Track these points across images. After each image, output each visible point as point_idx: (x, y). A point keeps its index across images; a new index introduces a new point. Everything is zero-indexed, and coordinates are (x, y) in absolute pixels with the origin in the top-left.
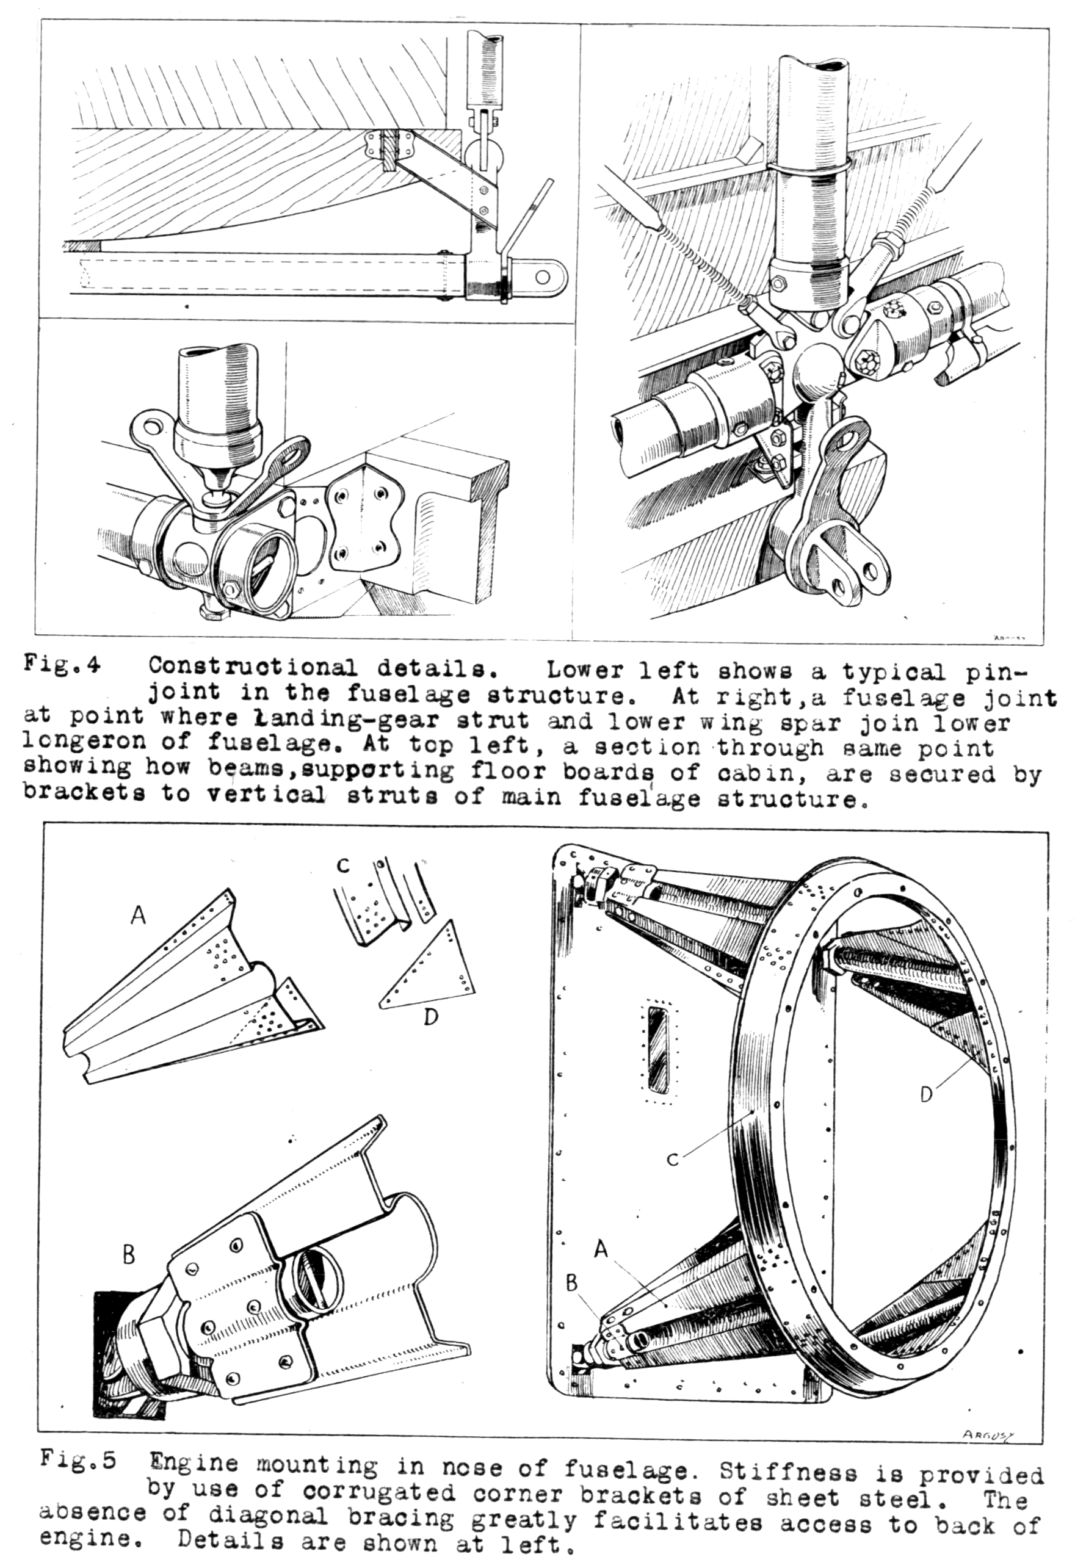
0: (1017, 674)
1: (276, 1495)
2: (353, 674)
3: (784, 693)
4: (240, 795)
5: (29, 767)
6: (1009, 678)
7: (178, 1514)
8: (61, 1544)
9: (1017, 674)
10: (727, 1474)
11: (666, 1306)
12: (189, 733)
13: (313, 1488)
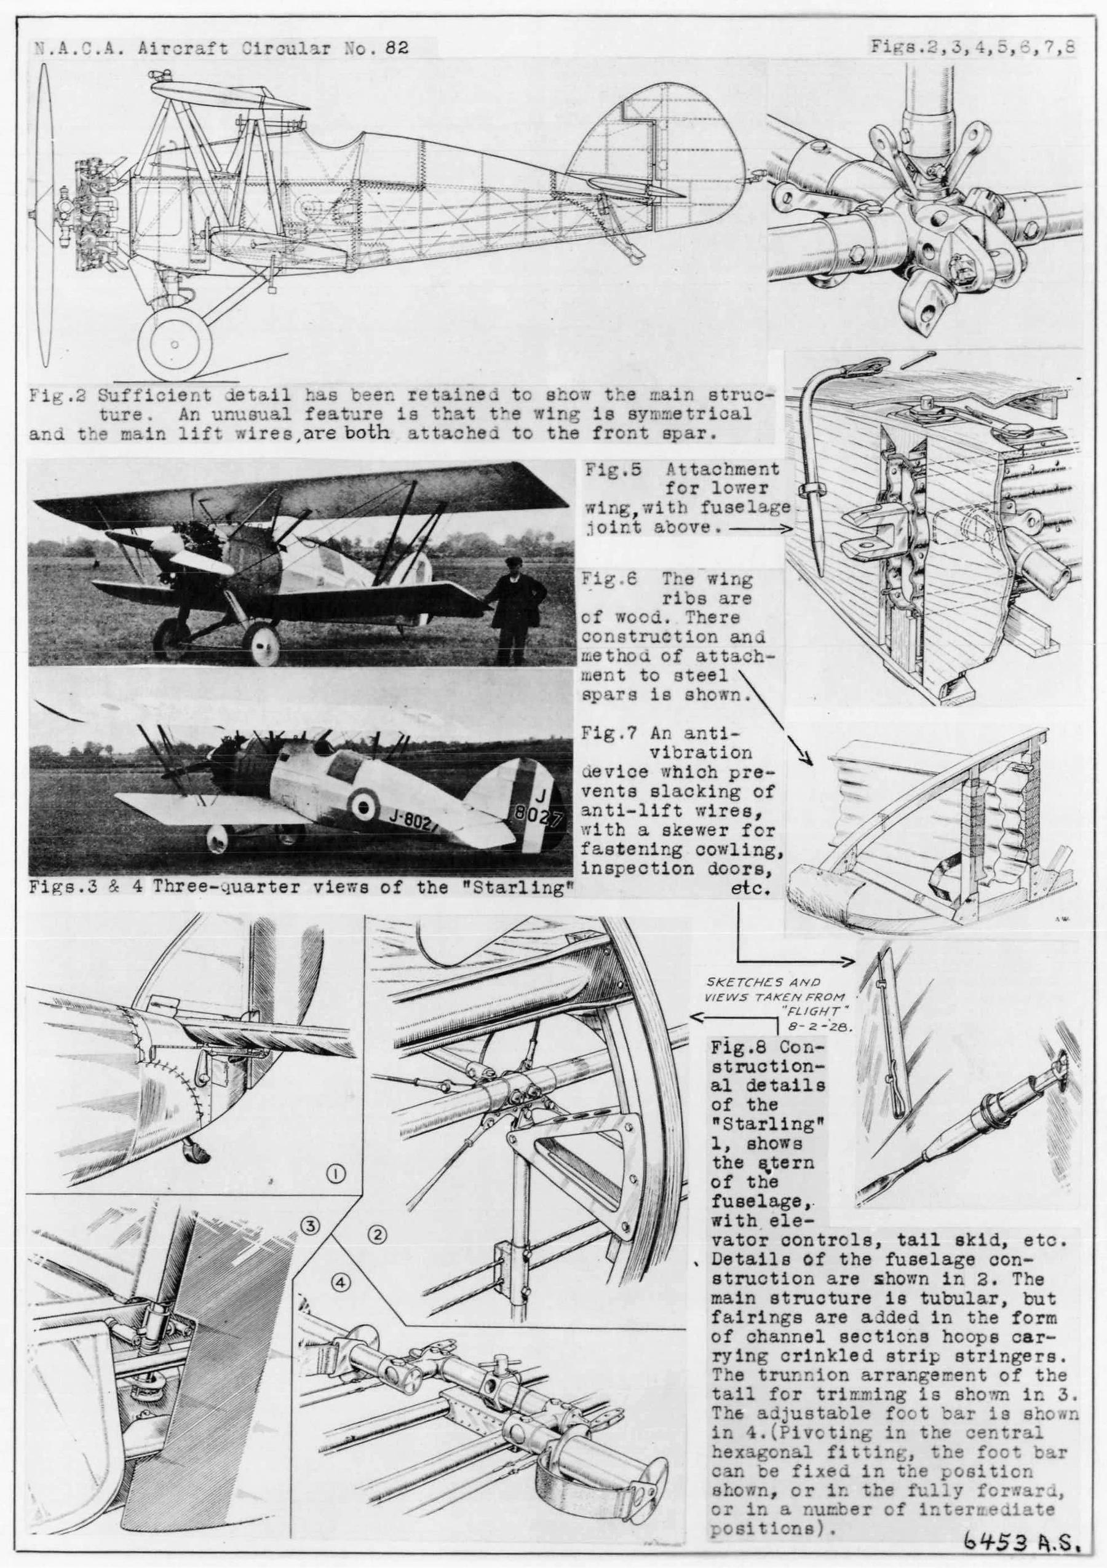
0: (817, 1067)
1: (820, 1264)
2: (728, 1090)
3: (1016, 1449)
4: (719, 619)
5: (717, 1491)
6: (811, 1071)
7: (724, 1106)
8: (815, 1092)
9: (817, 1067)
10: (728, 1126)
11: (735, 735)
12: (731, 1330)
13: (788, 1238)
